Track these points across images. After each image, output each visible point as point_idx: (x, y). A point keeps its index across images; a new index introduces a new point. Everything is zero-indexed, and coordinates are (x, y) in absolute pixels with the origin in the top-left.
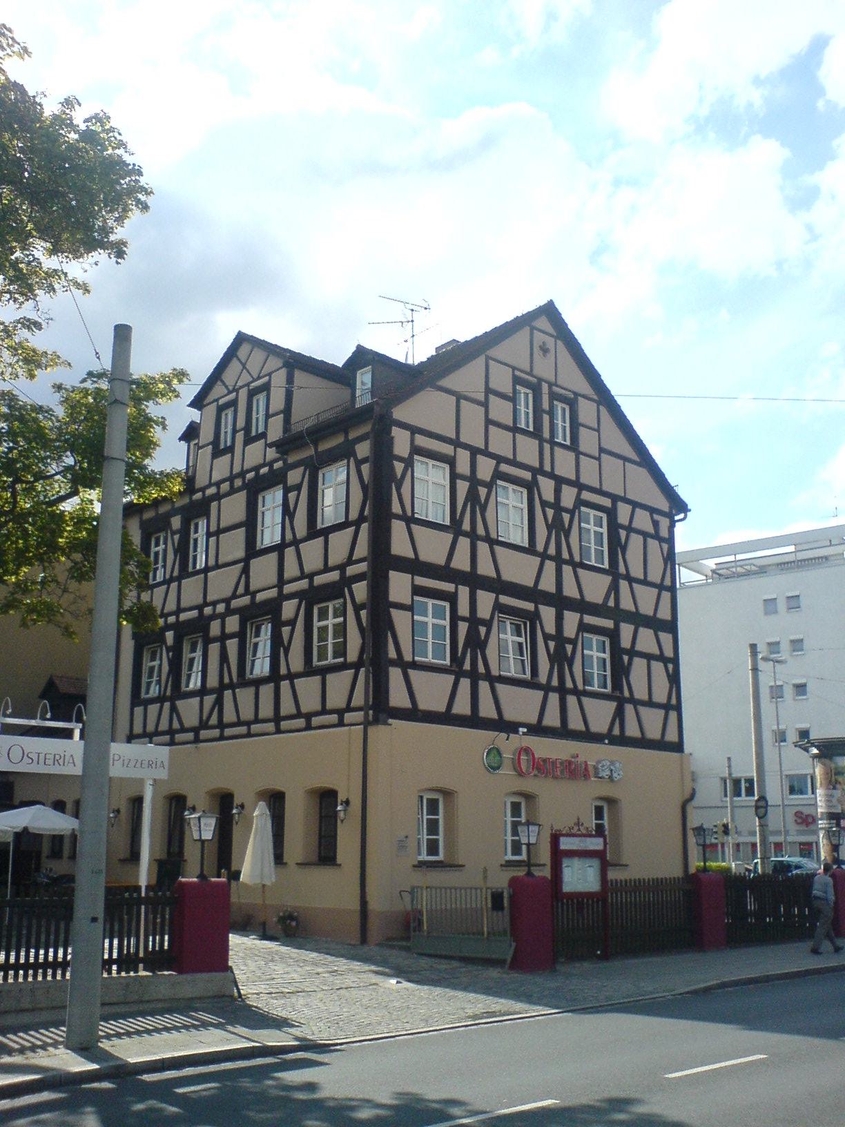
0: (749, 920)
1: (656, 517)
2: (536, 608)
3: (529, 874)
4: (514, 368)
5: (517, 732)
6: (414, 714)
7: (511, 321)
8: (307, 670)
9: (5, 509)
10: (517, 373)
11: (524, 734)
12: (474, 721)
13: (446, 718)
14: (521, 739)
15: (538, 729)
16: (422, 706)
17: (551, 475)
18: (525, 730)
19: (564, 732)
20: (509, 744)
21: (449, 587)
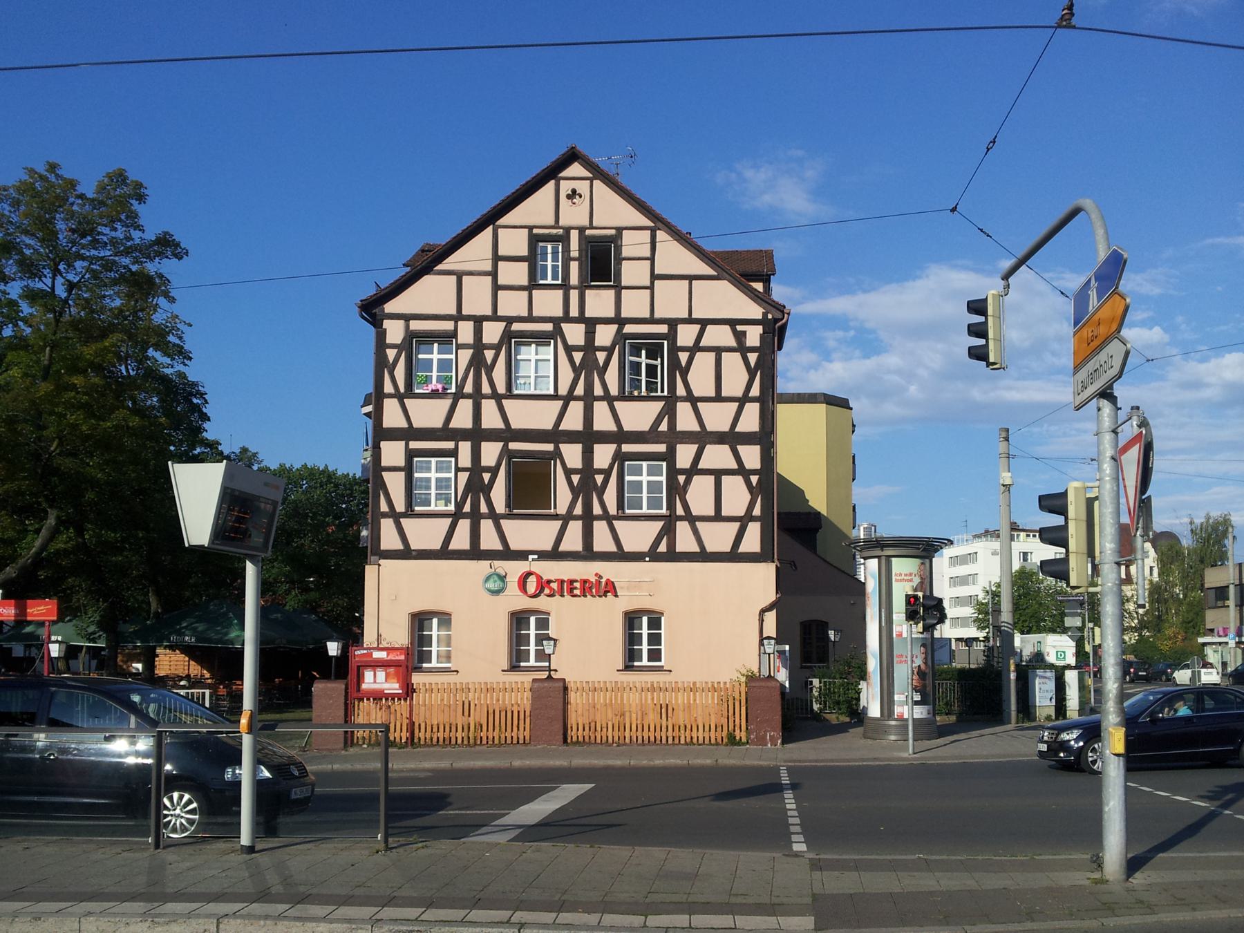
0: (63, 518)
1: (739, 328)
2: (557, 448)
3: (550, 677)
4: (530, 228)
5: (527, 559)
6: (406, 553)
7: (423, 276)
8: (507, 513)
9: (230, 770)
10: (535, 231)
11: (533, 560)
12: (475, 553)
13: (444, 553)
14: (532, 565)
15: (555, 554)
16: (627, 548)
17: (581, 319)
18: (536, 557)
19: (588, 553)
20: (514, 569)
21: (450, 445)
